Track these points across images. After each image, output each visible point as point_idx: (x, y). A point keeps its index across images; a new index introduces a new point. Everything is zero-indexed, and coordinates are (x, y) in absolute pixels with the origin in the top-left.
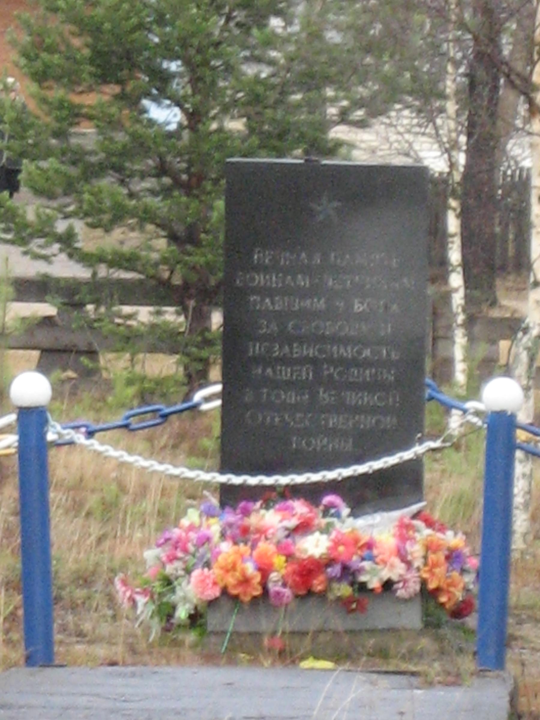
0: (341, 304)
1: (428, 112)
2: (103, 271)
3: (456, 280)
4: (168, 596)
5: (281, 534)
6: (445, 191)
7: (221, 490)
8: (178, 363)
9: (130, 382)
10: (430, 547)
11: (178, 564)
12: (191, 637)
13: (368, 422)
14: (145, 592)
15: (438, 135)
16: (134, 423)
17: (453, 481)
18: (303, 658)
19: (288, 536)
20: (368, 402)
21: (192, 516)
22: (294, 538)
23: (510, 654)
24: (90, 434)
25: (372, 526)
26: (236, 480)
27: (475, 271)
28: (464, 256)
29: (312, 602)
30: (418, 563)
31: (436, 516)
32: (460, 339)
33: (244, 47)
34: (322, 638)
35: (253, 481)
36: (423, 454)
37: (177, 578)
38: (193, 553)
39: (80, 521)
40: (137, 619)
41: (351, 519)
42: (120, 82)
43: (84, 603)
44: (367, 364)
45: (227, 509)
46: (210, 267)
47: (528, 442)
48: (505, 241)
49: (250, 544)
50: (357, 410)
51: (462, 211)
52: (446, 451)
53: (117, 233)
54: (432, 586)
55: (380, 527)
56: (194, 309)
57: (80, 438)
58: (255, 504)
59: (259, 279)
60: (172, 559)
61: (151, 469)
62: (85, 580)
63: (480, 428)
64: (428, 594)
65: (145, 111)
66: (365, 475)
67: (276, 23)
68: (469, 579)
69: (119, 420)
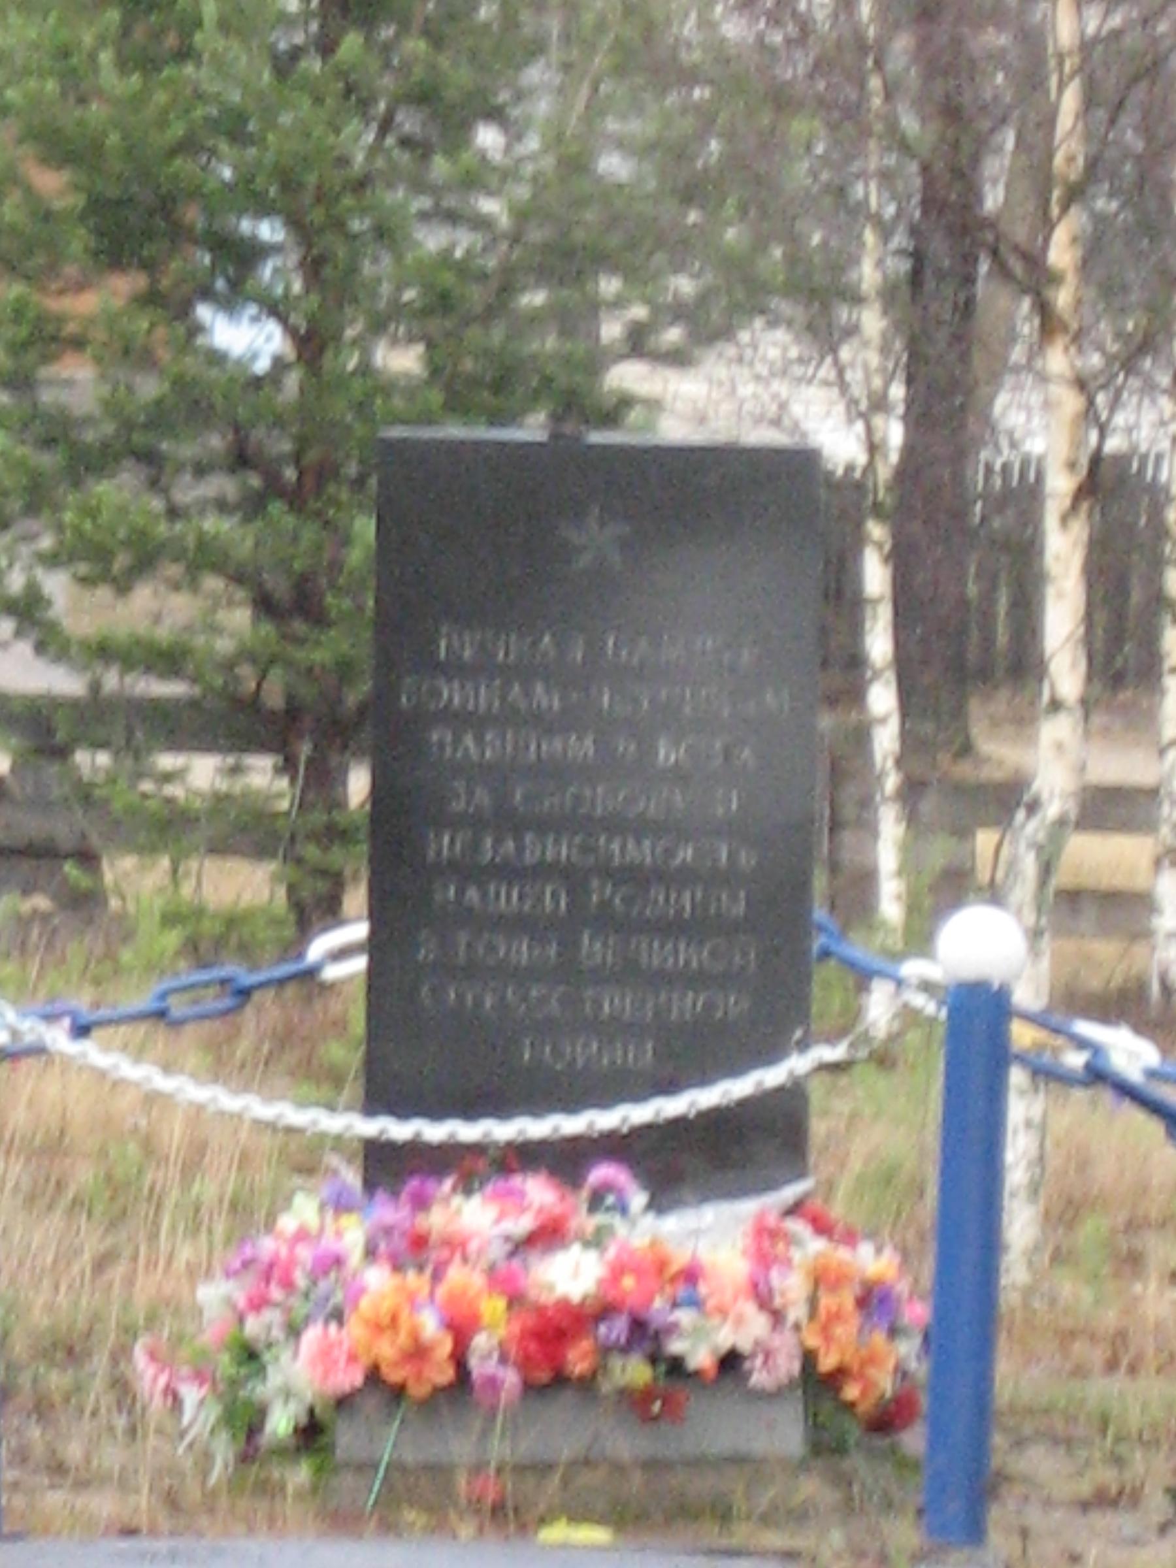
0: (625, 747)
1: (825, 335)
2: (111, 680)
3: (882, 698)
4: (249, 1386)
5: (497, 1251)
6: (858, 507)
7: (366, 1157)
8: (275, 878)
9: (170, 919)
10: (822, 1279)
11: (272, 1316)
12: (301, 1474)
13: (687, 1004)
14: (199, 1376)
15: (842, 385)
16: (178, 1006)
17: (879, 1131)
18: (543, 1521)
19: (512, 1254)
20: (687, 963)
21: (303, 1210)
22: (525, 1260)
23: (996, 1514)
24: (81, 1031)
25: (696, 1233)
26: (400, 1130)
27: (926, 679)
28: (898, 644)
29: (568, 1397)
30: (797, 1312)
31: (837, 1211)
32: (890, 828)
33: (419, 186)
34: (586, 1478)
35: (435, 1132)
36: (808, 1075)
37: (269, 1346)
38: (306, 1290)
39: (57, 1219)
40: (182, 1435)
41: (649, 1220)
42: (149, 266)
43: (67, 1400)
44: (686, 877)
45: (381, 1195)
46: (345, 670)
47: (1040, 1048)
48: (987, 616)
49: (429, 1271)
50: (662, 979)
51: (895, 547)
52: (857, 1070)
53: (144, 596)
54: (827, 1363)
55: (713, 1234)
56: (310, 761)
57: (58, 1038)
58: (440, 1182)
59: (451, 693)
60: (258, 1303)
61: (211, 1109)
62: (69, 1350)
63: (932, 1021)
64: (818, 1383)
65: (197, 329)
66: (678, 1124)
67: (488, 137)
68: (908, 1349)
69: (143, 1001)
